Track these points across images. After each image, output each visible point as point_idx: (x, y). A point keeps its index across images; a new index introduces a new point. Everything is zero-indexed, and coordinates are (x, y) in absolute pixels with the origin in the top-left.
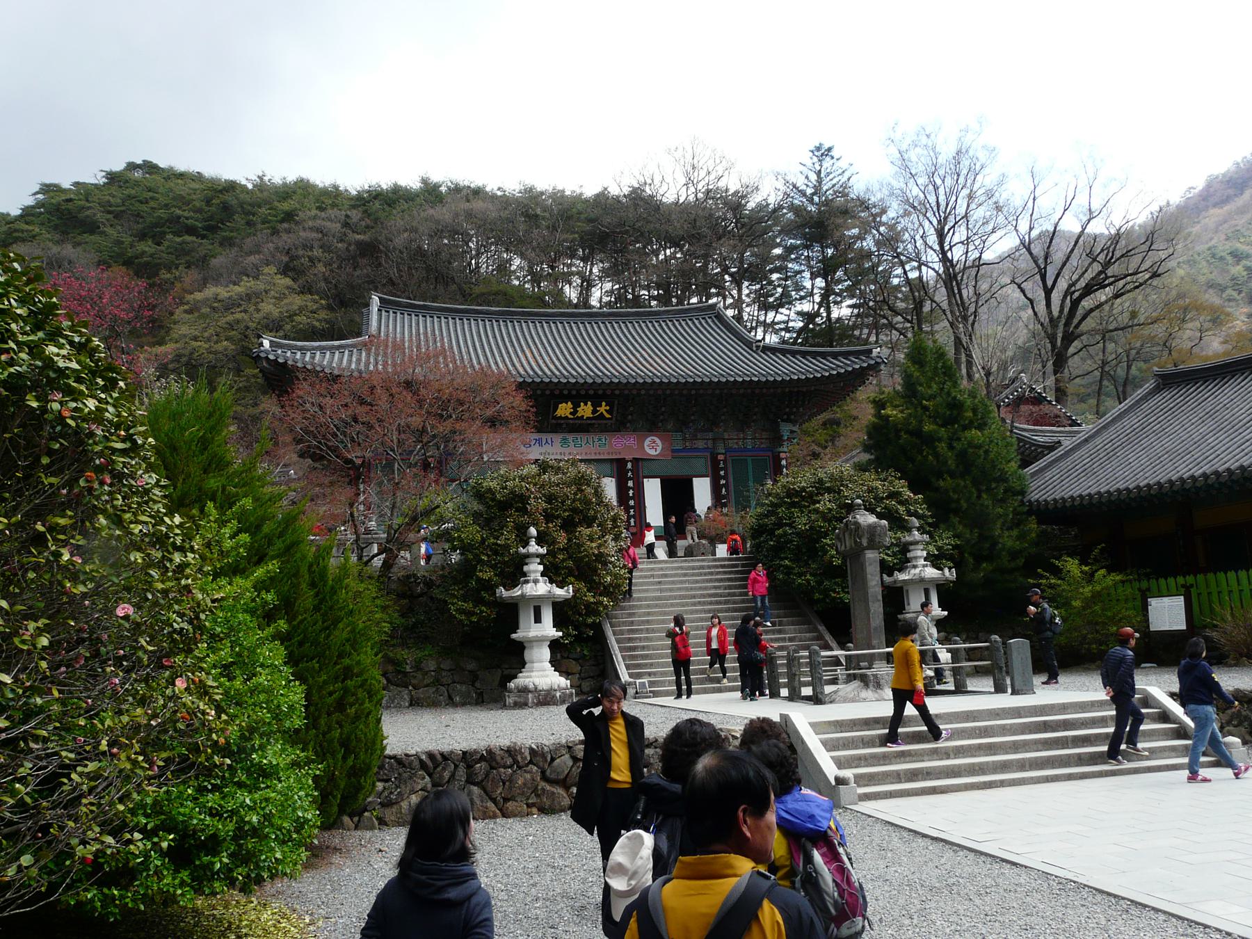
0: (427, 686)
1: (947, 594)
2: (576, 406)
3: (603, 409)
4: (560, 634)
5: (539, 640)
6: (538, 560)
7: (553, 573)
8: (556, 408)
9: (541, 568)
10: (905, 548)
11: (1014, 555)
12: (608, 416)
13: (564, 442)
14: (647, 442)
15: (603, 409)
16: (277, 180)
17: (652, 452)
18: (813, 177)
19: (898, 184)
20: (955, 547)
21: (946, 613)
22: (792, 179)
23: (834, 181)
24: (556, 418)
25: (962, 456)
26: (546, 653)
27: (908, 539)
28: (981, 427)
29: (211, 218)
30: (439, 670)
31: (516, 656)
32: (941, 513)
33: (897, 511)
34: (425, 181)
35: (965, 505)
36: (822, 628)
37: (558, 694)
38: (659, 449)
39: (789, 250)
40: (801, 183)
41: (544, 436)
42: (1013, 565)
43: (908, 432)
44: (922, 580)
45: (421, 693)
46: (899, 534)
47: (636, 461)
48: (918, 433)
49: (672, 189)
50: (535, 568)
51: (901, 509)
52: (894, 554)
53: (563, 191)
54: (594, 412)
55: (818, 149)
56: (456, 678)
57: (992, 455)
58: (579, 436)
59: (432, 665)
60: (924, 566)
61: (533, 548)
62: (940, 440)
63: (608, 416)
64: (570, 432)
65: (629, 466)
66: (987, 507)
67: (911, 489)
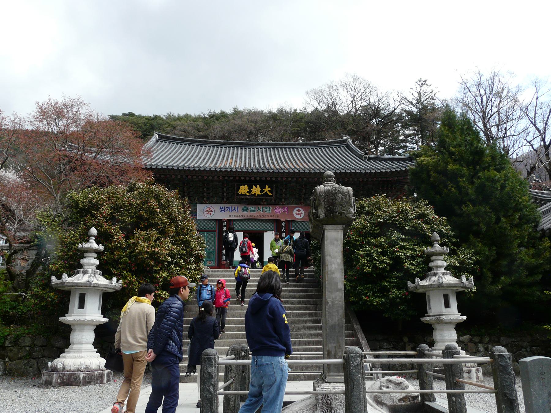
0: (21, 358)
1: (465, 301)
2: (250, 188)
3: (267, 189)
4: (107, 320)
5: (83, 324)
6: (95, 255)
7: (105, 269)
8: (238, 189)
9: (97, 262)
10: (428, 258)
11: (532, 270)
12: (270, 194)
13: (245, 209)
14: (295, 211)
15: (267, 189)
16: (176, 115)
17: (298, 217)
18: (416, 95)
19: (460, 96)
20: (476, 263)
21: (465, 318)
22: (404, 95)
23: (427, 97)
24: (238, 195)
25: (481, 190)
26: (90, 336)
27: (430, 249)
28: (498, 170)
29: (146, 131)
30: (33, 346)
31: (60, 338)
32: (462, 236)
33: (422, 229)
34: (235, 110)
35: (484, 229)
36: (357, 327)
37: (82, 375)
38: (302, 215)
39: (408, 136)
40: (410, 98)
41: (233, 206)
42: (530, 279)
43: (436, 172)
44: (440, 286)
45: (13, 365)
46: (424, 248)
47: (288, 222)
48: (444, 173)
49: (345, 105)
50: (91, 261)
51: (426, 227)
52: (418, 264)
53: (296, 110)
54: (262, 191)
55: (420, 81)
56: (46, 353)
57: (508, 189)
58: (254, 206)
59: (27, 341)
60: (444, 274)
61: (92, 244)
62: (462, 176)
63: (270, 194)
64: (249, 204)
65: (283, 224)
66: (505, 229)
67: (437, 212)
